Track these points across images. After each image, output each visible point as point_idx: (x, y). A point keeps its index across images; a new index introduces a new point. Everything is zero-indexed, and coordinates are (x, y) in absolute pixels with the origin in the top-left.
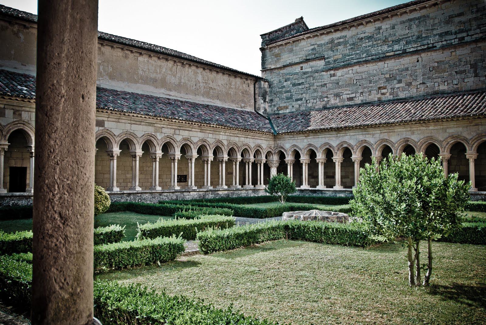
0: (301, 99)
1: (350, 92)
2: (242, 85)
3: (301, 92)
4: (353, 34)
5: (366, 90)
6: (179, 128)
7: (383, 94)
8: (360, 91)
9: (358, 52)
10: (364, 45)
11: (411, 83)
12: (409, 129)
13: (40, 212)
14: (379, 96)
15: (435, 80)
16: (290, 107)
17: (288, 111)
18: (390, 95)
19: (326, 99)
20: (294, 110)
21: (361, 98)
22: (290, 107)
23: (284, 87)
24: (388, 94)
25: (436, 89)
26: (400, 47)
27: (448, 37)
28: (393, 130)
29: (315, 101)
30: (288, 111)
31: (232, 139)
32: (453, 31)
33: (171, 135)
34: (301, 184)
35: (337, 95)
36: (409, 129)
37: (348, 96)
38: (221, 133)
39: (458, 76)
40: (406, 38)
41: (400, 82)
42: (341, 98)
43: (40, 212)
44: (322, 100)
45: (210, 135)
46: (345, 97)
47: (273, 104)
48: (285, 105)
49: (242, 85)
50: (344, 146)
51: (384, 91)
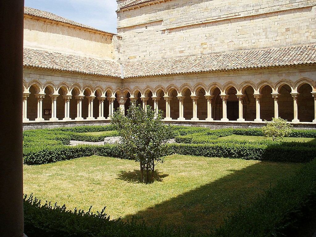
0: (146, 51)
1: (181, 47)
2: (101, 39)
3: (146, 46)
4: (184, 3)
5: (192, 45)
6: (43, 74)
7: (204, 48)
8: (188, 46)
9: (187, 16)
10: (191, 11)
11: (223, 41)
12: (217, 76)
13: (179, 144)
14: (202, 50)
15: (240, 40)
16: (138, 57)
17: (136, 60)
18: (210, 49)
19: (164, 51)
20: (140, 59)
21: (189, 51)
22: (138, 57)
23: (133, 41)
24: (208, 49)
25: (241, 46)
26: (216, 14)
27: (248, 9)
28: (206, 77)
29: (156, 53)
30: (136, 60)
31: (87, 81)
32: (252, 5)
33: (37, 79)
34: (164, 116)
35: (172, 49)
36: (217, 76)
37: (180, 50)
38: (78, 78)
39: (255, 37)
40: (220, 7)
41: (216, 40)
42: (175, 51)
43: (179, 144)
44: (161, 52)
45: (69, 80)
46: (177, 50)
47: (125, 54)
48: (134, 55)
49: (101, 39)
50: (172, 88)
51: (205, 46)
